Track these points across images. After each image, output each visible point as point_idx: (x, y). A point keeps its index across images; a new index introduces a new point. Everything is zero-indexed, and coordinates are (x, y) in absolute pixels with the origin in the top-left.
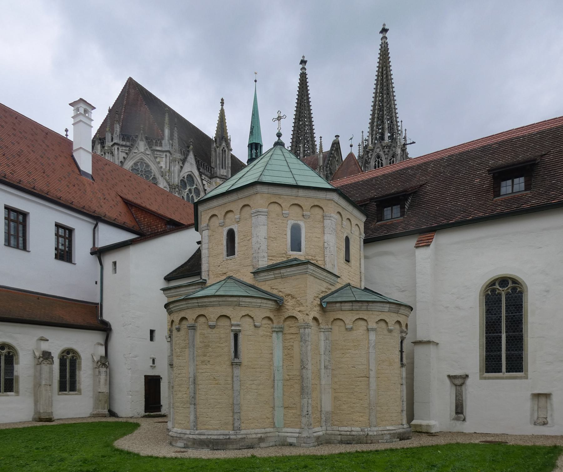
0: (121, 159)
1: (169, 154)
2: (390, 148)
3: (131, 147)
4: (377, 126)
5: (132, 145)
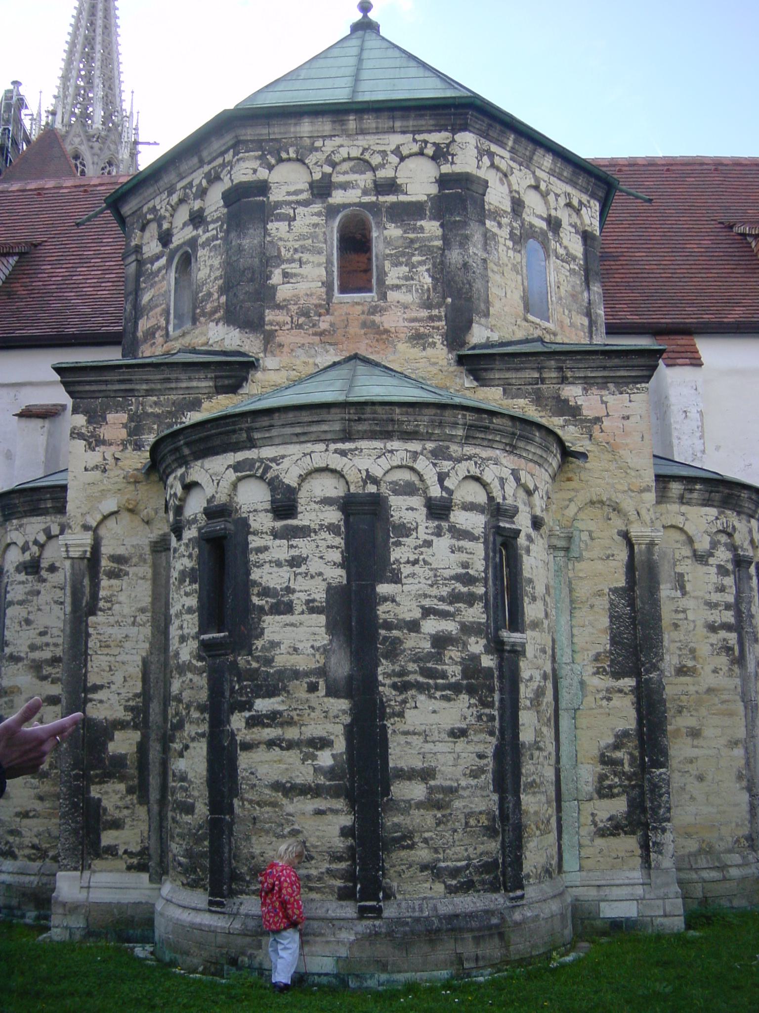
2: (104, 143)
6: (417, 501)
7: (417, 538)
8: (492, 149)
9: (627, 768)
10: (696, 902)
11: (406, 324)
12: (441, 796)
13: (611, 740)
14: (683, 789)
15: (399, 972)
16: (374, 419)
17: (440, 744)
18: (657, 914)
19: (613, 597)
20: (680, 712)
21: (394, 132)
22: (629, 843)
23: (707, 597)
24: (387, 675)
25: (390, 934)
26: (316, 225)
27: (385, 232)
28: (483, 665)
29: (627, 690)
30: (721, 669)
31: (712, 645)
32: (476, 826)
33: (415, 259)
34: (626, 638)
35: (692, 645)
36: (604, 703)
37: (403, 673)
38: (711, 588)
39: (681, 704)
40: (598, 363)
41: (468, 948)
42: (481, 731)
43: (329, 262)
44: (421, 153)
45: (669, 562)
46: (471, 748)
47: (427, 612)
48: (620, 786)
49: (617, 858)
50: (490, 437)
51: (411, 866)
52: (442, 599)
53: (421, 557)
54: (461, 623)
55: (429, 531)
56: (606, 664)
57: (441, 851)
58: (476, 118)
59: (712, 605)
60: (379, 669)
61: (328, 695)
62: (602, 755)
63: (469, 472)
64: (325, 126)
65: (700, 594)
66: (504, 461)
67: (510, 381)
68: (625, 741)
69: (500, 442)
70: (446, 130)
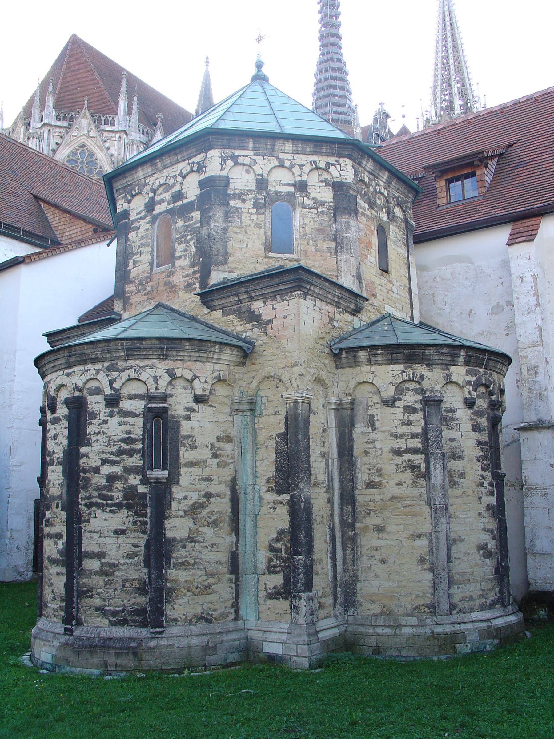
0: (53, 146)
1: (125, 136)
3: (68, 129)
4: (442, 91)
5: (70, 124)
6: (100, 398)
7: (100, 419)
8: (236, 154)
9: (283, 554)
10: (371, 649)
11: (184, 279)
12: (108, 569)
13: (275, 535)
14: (370, 568)
15: (75, 667)
16: (76, 354)
17: (109, 539)
18: (293, 654)
19: (278, 440)
20: (369, 514)
21: (179, 162)
22: (283, 604)
23: (393, 430)
24: (83, 499)
25: (73, 645)
26: (147, 230)
27: (177, 225)
28: (139, 491)
29: (284, 502)
30: (405, 482)
31: (397, 465)
32: (130, 587)
33: (189, 237)
34: (284, 467)
35: (379, 466)
36: (272, 510)
37: (90, 497)
38: (397, 423)
39: (369, 508)
40: (267, 284)
41: (111, 659)
42: (136, 531)
43: (152, 250)
44: (192, 171)
45: (363, 408)
46: (128, 541)
47: (104, 462)
48: (279, 566)
49: (278, 614)
50: (144, 353)
51: (90, 608)
52: (112, 454)
53: (102, 430)
54: (123, 467)
55: (106, 415)
56: (273, 485)
57: (107, 600)
58: (216, 139)
59: (397, 436)
60: (80, 495)
61: (62, 510)
62: (270, 545)
63: (129, 376)
64: (148, 169)
65: (388, 428)
66: (159, 366)
67: (225, 305)
68: (282, 536)
69: (153, 354)
70: (203, 152)
